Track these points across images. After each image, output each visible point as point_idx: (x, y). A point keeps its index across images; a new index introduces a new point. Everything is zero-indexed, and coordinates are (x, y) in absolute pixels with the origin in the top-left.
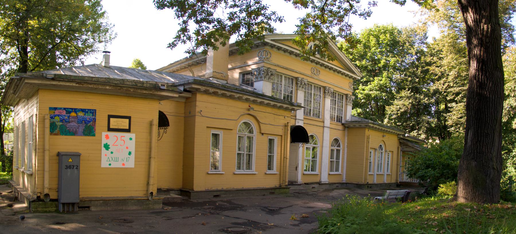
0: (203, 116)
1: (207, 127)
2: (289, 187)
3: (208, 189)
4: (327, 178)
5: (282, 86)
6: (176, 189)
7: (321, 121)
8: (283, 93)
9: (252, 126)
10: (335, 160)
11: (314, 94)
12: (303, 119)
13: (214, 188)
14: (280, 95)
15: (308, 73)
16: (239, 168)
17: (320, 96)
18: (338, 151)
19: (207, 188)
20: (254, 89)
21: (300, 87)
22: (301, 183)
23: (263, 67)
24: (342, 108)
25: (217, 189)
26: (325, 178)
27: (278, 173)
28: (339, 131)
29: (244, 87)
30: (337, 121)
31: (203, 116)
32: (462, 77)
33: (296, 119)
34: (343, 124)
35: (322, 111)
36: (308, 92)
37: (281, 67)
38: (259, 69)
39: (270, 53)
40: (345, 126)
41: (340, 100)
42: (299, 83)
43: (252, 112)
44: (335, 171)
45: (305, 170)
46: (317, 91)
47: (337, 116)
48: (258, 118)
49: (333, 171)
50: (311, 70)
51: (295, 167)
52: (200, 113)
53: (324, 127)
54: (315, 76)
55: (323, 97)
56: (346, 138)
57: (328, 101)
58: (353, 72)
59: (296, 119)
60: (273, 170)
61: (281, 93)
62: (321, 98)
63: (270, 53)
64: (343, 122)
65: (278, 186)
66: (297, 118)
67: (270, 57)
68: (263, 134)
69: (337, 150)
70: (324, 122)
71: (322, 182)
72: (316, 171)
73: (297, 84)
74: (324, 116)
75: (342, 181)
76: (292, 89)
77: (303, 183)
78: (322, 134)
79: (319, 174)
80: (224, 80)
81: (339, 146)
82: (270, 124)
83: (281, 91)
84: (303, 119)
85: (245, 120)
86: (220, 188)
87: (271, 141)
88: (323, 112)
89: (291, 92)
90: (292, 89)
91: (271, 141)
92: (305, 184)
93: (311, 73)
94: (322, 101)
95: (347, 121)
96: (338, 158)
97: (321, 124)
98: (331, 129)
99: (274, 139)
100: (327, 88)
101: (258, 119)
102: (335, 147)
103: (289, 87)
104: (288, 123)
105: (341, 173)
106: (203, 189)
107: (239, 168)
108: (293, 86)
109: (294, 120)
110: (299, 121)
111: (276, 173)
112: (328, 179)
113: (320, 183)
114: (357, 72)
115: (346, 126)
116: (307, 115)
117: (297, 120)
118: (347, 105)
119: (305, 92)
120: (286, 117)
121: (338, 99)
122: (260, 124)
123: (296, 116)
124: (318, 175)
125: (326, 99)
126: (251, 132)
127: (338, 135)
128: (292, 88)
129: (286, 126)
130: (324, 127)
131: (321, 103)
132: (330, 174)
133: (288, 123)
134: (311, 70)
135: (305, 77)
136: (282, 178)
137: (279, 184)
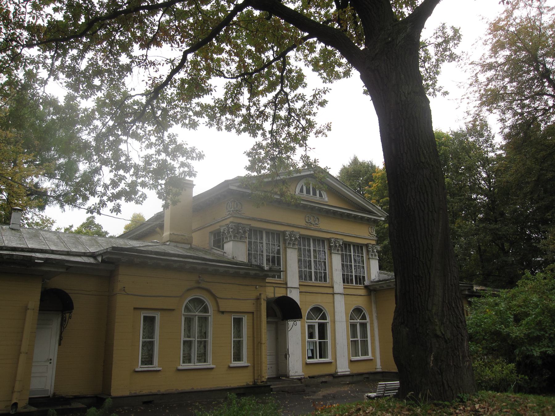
0: (128, 294)
1: (135, 309)
2: (269, 384)
3: (136, 393)
4: (348, 367)
5: (262, 246)
6: (89, 396)
7: (329, 286)
8: (265, 254)
9: (206, 302)
10: (359, 338)
11: (315, 251)
12: (297, 286)
13: (145, 392)
14: (261, 257)
15: (303, 223)
16: (188, 359)
17: (325, 251)
18: (364, 326)
19: (133, 392)
20: (224, 252)
21: (289, 243)
22: (303, 377)
23: (232, 222)
24: (364, 264)
25: (151, 392)
26: (343, 367)
27: (249, 365)
28: (362, 297)
29: (215, 251)
30: (356, 283)
31: (128, 294)
32: (143, 65)
33: (287, 288)
34: (366, 287)
35: (329, 272)
36: (304, 249)
37: (259, 221)
38: (227, 226)
39: (241, 203)
40: (370, 289)
41: (358, 253)
42: (287, 238)
43: (203, 285)
44: (362, 355)
45: (309, 358)
46: (319, 245)
47: (356, 276)
48: (213, 291)
49: (359, 356)
50: (305, 219)
51: (285, 354)
52: (124, 290)
53: (333, 294)
54: (312, 226)
55: (329, 253)
56: (374, 310)
57: (337, 261)
58: (370, 212)
59: (287, 288)
60: (243, 361)
61: (262, 255)
62: (326, 254)
63: (241, 203)
64: (367, 283)
65: (251, 384)
66: (289, 285)
67: (242, 208)
68: (223, 312)
69: (200, 318)
70: (333, 287)
71: (339, 374)
72: (328, 358)
73: (285, 240)
74: (332, 279)
75: (376, 369)
76: (279, 248)
77: (307, 376)
78: (332, 304)
79: (333, 361)
80: (186, 244)
81: (364, 318)
82: (234, 298)
83: (262, 252)
84: (297, 286)
85: (195, 296)
86: (154, 391)
87: (238, 322)
88: (330, 274)
89: (279, 252)
90: (279, 248)
91: (238, 322)
92: (309, 377)
93: (305, 223)
94: (328, 259)
95: (372, 282)
96: (364, 334)
97: (329, 291)
98: (346, 296)
99: (242, 318)
100: (332, 240)
101: (214, 293)
102: (357, 320)
103: (274, 245)
104: (260, 294)
105: (371, 358)
106: (127, 393)
107: (188, 359)
108: (279, 243)
109: (285, 289)
110: (291, 289)
111: (246, 364)
112: (349, 368)
113: (335, 376)
114: (377, 211)
115: (371, 288)
116: (348, 283)
117: (288, 290)
118: (369, 259)
119: (300, 250)
120: (257, 287)
121: (354, 252)
122: (218, 299)
123: (286, 284)
124: (331, 363)
125: (333, 255)
126: (206, 310)
127: (361, 302)
128: (279, 246)
129: (258, 299)
130: (333, 294)
131: (326, 261)
132: (353, 360)
133: (260, 294)
134: (305, 219)
135: (296, 230)
136: (256, 372)
137: (252, 380)
